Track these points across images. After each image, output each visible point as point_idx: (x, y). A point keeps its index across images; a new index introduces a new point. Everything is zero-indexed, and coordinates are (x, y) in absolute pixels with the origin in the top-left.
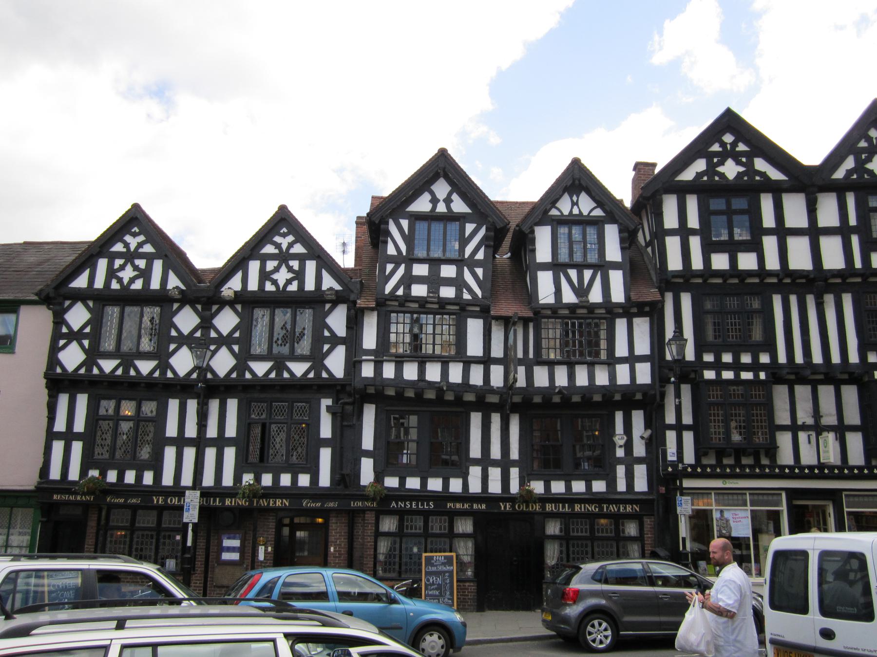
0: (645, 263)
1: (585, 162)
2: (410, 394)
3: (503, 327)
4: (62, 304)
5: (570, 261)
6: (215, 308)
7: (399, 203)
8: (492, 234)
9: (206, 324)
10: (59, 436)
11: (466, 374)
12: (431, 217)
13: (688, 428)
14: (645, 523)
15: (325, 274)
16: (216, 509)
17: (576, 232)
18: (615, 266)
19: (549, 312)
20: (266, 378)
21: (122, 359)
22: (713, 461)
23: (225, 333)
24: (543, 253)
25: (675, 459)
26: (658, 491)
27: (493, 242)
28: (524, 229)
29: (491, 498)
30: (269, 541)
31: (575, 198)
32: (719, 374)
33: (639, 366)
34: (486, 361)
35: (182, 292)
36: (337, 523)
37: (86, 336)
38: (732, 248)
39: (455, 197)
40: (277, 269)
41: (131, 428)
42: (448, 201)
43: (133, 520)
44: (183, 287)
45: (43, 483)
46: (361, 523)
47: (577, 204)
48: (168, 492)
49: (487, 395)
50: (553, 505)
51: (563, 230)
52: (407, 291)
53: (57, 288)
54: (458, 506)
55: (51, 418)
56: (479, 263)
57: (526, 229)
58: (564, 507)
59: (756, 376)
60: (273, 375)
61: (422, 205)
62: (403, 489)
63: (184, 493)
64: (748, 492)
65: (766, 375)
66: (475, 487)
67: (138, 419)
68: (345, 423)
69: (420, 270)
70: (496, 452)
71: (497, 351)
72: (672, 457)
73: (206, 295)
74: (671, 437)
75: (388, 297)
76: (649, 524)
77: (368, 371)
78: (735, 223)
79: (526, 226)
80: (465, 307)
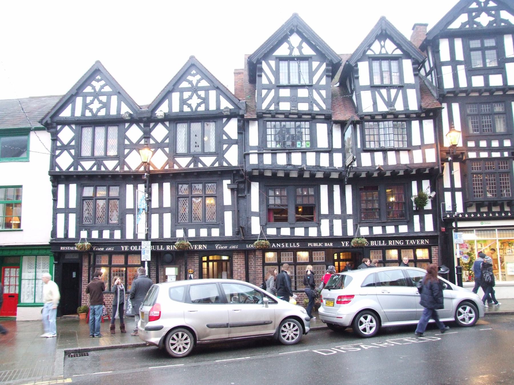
0: (426, 86)
1: (389, 19)
2: (281, 174)
3: (340, 129)
4: (56, 128)
5: (382, 83)
6: (152, 125)
7: (268, 50)
8: (330, 68)
9: (147, 136)
10: (61, 211)
11: (318, 159)
12: (289, 59)
13: (458, 190)
14: (432, 250)
15: (222, 99)
16: (160, 252)
17: (385, 64)
18: (411, 86)
19: (369, 118)
20: (187, 168)
21: (96, 160)
22: (474, 210)
23: (159, 150)
24: (364, 79)
25: (451, 209)
26: (440, 230)
27: (331, 73)
28: (351, 64)
29: (336, 239)
30: (196, 271)
31: (382, 43)
32: (478, 154)
33: (427, 151)
34: (330, 151)
35: (130, 115)
36: (238, 259)
37: (73, 147)
38: (486, 72)
39: (304, 45)
40: (190, 98)
41: (104, 204)
42: (300, 47)
43: (110, 261)
44: (132, 113)
45: (53, 240)
46: (253, 258)
47: (384, 47)
48: (130, 243)
49: (332, 173)
50: (375, 241)
51: (376, 64)
52: (277, 107)
53: (52, 117)
54: (315, 245)
55: (55, 200)
56: (323, 87)
57: (352, 63)
58: (382, 243)
59: (502, 154)
60: (217, 165)
61: (283, 51)
62: (279, 236)
63: (141, 243)
64: (496, 229)
65: (509, 154)
66: (325, 233)
67: (108, 199)
68: (240, 195)
69: (285, 93)
70: (337, 210)
71: (337, 144)
72: (448, 207)
73: (146, 116)
74: (448, 196)
75: (264, 111)
76: (435, 251)
77: (253, 160)
78: (487, 56)
79: (353, 61)
80: (315, 116)
